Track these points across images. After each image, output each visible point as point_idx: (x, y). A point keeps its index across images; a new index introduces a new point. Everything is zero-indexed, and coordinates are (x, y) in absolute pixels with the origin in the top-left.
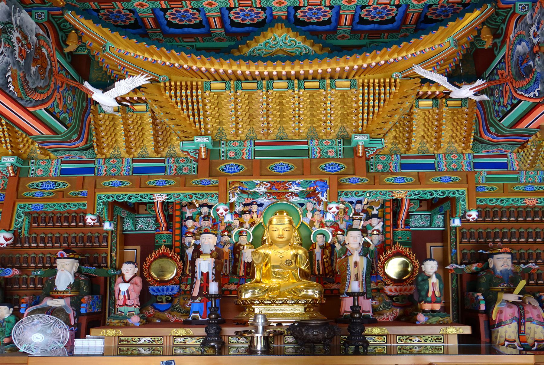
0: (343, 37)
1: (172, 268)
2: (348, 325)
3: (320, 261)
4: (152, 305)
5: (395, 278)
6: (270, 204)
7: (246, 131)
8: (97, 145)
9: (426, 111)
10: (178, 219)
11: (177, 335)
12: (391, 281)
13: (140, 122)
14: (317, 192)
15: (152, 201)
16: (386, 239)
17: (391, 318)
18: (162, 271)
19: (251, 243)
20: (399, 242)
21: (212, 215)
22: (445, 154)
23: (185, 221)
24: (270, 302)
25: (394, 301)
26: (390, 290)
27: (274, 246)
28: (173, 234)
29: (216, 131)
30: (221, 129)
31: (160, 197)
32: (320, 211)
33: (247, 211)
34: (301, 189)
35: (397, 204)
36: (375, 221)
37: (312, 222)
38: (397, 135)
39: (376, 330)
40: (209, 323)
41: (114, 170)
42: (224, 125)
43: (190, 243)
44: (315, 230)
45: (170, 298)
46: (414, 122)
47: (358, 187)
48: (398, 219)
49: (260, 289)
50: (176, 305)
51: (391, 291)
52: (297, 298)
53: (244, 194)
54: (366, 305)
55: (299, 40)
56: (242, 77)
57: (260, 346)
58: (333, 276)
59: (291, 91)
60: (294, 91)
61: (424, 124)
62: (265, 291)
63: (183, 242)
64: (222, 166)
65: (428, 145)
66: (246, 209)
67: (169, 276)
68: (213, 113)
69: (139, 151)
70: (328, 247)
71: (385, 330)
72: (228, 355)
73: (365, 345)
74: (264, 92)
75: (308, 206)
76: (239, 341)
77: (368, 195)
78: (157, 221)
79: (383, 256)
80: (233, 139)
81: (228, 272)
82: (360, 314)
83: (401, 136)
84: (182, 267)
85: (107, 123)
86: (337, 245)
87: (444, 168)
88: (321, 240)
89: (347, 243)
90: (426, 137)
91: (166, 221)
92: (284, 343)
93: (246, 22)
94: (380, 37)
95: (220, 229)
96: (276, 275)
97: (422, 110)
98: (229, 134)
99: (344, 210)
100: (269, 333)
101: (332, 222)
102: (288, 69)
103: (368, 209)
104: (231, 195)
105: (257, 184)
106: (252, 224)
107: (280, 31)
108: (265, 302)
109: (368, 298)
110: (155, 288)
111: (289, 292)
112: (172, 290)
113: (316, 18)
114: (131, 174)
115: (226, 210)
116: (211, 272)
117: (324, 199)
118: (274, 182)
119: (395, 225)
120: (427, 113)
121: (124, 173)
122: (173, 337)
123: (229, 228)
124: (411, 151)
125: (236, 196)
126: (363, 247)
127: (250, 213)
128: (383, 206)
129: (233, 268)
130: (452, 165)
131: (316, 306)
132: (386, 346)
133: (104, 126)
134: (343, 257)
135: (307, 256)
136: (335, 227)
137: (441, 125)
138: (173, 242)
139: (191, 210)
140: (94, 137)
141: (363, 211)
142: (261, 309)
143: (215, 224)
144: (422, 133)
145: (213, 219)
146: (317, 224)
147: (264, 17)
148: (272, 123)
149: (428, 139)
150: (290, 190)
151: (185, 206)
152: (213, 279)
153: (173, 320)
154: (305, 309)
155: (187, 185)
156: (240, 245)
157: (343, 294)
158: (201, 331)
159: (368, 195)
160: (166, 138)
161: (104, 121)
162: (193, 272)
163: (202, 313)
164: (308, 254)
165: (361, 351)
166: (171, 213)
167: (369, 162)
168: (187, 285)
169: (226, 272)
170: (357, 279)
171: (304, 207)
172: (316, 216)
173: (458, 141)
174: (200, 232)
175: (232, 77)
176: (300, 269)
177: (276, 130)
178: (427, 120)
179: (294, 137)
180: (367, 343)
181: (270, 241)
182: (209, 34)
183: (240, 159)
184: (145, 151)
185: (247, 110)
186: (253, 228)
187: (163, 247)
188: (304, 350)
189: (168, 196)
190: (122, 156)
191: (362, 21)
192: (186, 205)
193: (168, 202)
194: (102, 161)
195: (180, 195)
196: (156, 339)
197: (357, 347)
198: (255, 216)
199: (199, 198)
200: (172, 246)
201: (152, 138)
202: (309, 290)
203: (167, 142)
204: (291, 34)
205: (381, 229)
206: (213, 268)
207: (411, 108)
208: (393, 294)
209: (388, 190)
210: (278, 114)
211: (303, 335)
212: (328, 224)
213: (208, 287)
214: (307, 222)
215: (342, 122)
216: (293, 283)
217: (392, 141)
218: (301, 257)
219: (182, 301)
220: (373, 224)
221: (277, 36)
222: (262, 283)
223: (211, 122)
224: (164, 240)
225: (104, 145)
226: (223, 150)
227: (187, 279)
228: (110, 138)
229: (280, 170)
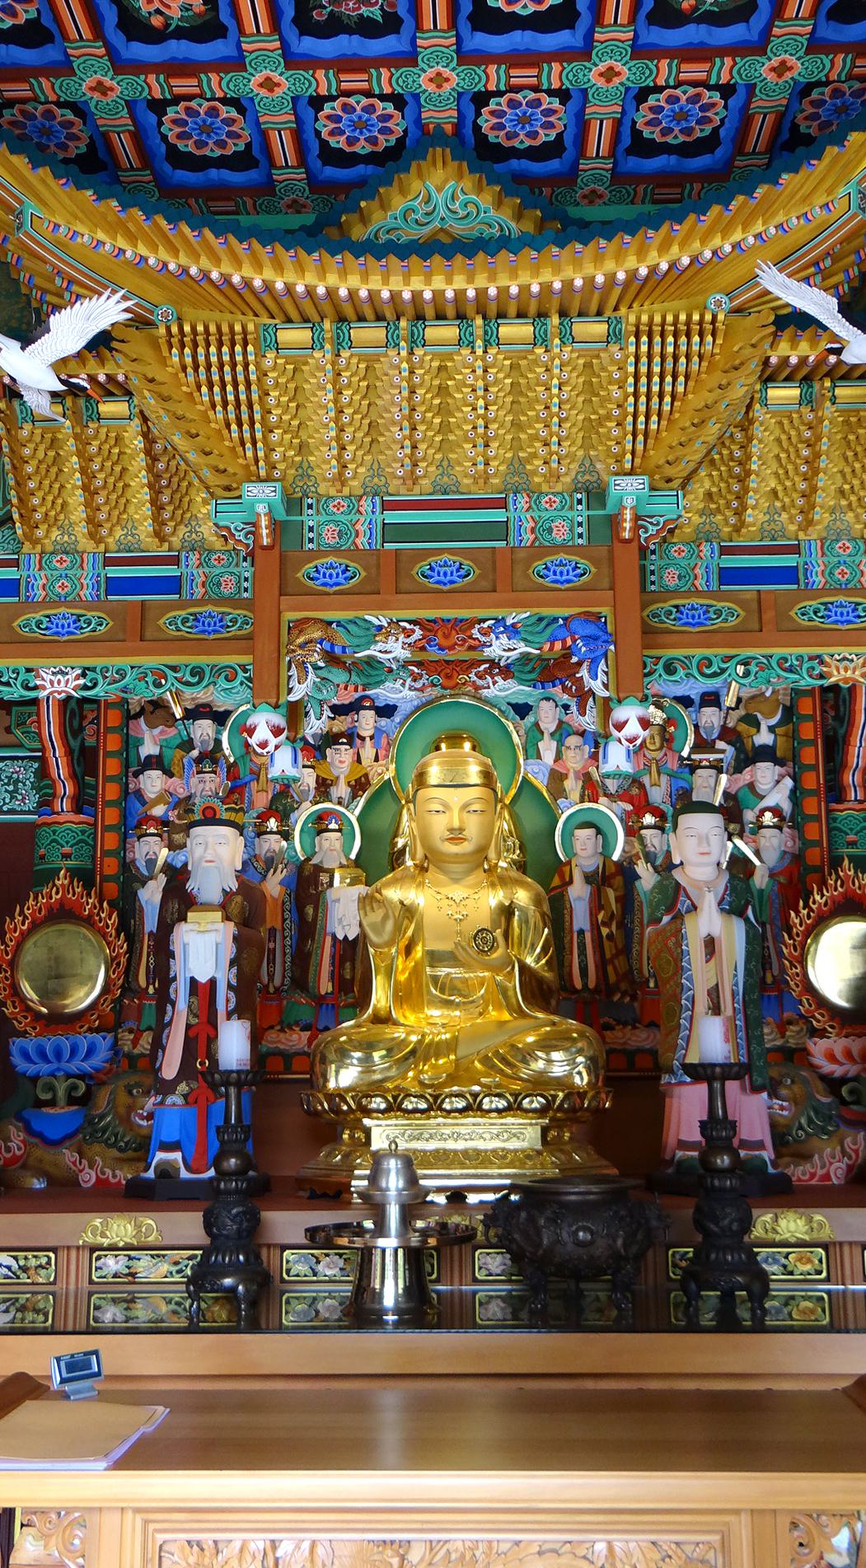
0: (592, 197)
1: (91, 960)
2: (693, 1201)
3: (588, 936)
4: (19, 1118)
5: (843, 1004)
6: (418, 708)
7: (362, 470)
8: (21, 515)
9: (784, 415)
10: (112, 767)
11: (106, 1242)
12: (832, 1019)
13: (116, 450)
14: (575, 659)
15: (32, 694)
16: (806, 844)
17: (837, 1171)
18: (56, 979)
19: (357, 863)
20: (852, 858)
21: (227, 752)
22: (823, 540)
23: (136, 775)
24: (423, 1105)
25: (843, 1102)
26: (829, 1052)
27: (433, 873)
28: (95, 825)
29: (293, 471)
30: (305, 465)
31: (57, 681)
32: (582, 734)
33: (342, 735)
34: (523, 648)
35: (836, 707)
36: (765, 773)
37: (557, 778)
38: (714, 490)
39: (792, 1225)
40: (218, 1192)
41: (63, 586)
42: (312, 454)
43: (151, 863)
44: (568, 810)
45: (82, 1087)
47: (708, 639)
48: (844, 765)
49: (389, 1050)
50: (102, 1117)
51: (831, 1057)
52: (516, 1087)
53: (334, 670)
54: (753, 1114)
55: (485, 200)
56: (349, 311)
57: (391, 1290)
58: (634, 997)
59: (466, 352)
60: (473, 352)
61: (777, 457)
62: (406, 1058)
63: (130, 856)
64: (309, 568)
65: (784, 516)
66: (341, 724)
67: (82, 997)
68: (286, 417)
69: (119, 533)
70: (613, 876)
71: (821, 1225)
72: (281, 1329)
73: (756, 1287)
74: (404, 353)
75: (542, 714)
76: (320, 1268)
77: (741, 669)
78: (43, 773)
79: (797, 913)
80: (333, 492)
81: (277, 981)
82: (734, 1153)
83: (724, 492)
84: (123, 960)
85: (40, 454)
86: (642, 868)
87: (818, 580)
88: (590, 851)
89: (676, 861)
90: (781, 494)
91: (73, 775)
92: (475, 1281)
93: (357, 149)
94: (682, 194)
95: (251, 804)
96: (442, 991)
97: (774, 414)
98: (324, 479)
99: (663, 729)
100: (425, 1233)
101: (627, 776)
103: (742, 727)
104: (294, 671)
105: (380, 628)
106: (359, 785)
107: (439, 174)
108: (408, 1105)
109: (756, 1090)
110: (30, 1044)
111: (485, 1060)
112: (90, 1052)
113: (528, 135)
114: (102, 597)
115: (277, 732)
116: (225, 977)
117: (597, 686)
118: (434, 621)
119: (835, 792)
120: (786, 422)
121: (86, 594)
122: (93, 1249)
123: (283, 801)
124: (744, 530)
125: (311, 676)
126: (732, 877)
127: (350, 743)
128: (789, 713)
129: (301, 969)
130: (837, 571)
131: (576, 1121)
132: (829, 1292)
133: (34, 463)
134: (666, 919)
135: (543, 915)
136: (634, 795)
137: (817, 455)
138: (94, 857)
139: (156, 731)
140: (13, 492)
141: (726, 733)
142: (393, 1132)
143: (236, 790)
144: (773, 484)
145: (230, 766)
146: (572, 786)
147: (399, 131)
148: (422, 447)
149: (787, 500)
150: (488, 652)
151: (137, 716)
152: (232, 1006)
153: (88, 1178)
154: (545, 1131)
155: (148, 635)
156: (319, 869)
157: (671, 1071)
158: (188, 1226)
159: (741, 669)
160: (178, 496)
161: (32, 446)
162: (163, 975)
163: (191, 1149)
164: (546, 908)
165: (743, 1313)
166: (90, 742)
167: (647, 563)
168: (138, 1034)
169: (271, 977)
170: (716, 1010)
171: (530, 719)
172: (570, 754)
173: (854, 505)
174: (188, 817)
175: (327, 307)
176: (524, 968)
177: (432, 469)
178: (785, 444)
179: (473, 488)
180: (763, 1277)
181: (420, 853)
182: (268, 187)
183: (349, 550)
184: (133, 535)
185: (364, 409)
186: (362, 802)
187: (62, 880)
188: (545, 1307)
189: (84, 675)
190: (80, 548)
191: (642, 147)
192: (142, 712)
193: (85, 700)
194: (35, 560)
195: (128, 674)
196: (33, 1262)
197: (728, 1297)
198: (368, 752)
199: (188, 684)
200: (93, 872)
201: (145, 495)
202: (556, 1055)
203: (181, 504)
204: (468, 182)
205: (786, 807)
206: (232, 963)
207: (749, 407)
208: (838, 1071)
209: (805, 651)
210: (437, 421)
211: (540, 1244)
212: (612, 785)
213: (213, 1038)
214: (537, 774)
215: (586, 445)
216: (502, 1024)
217: (701, 506)
218: (525, 921)
219: (123, 1099)
220: (762, 787)
221: (432, 189)
222: (396, 1023)
223: (281, 444)
224: (67, 849)
225: (38, 516)
226: (311, 523)
227: (140, 1008)
228: (50, 498)
229: (442, 578)
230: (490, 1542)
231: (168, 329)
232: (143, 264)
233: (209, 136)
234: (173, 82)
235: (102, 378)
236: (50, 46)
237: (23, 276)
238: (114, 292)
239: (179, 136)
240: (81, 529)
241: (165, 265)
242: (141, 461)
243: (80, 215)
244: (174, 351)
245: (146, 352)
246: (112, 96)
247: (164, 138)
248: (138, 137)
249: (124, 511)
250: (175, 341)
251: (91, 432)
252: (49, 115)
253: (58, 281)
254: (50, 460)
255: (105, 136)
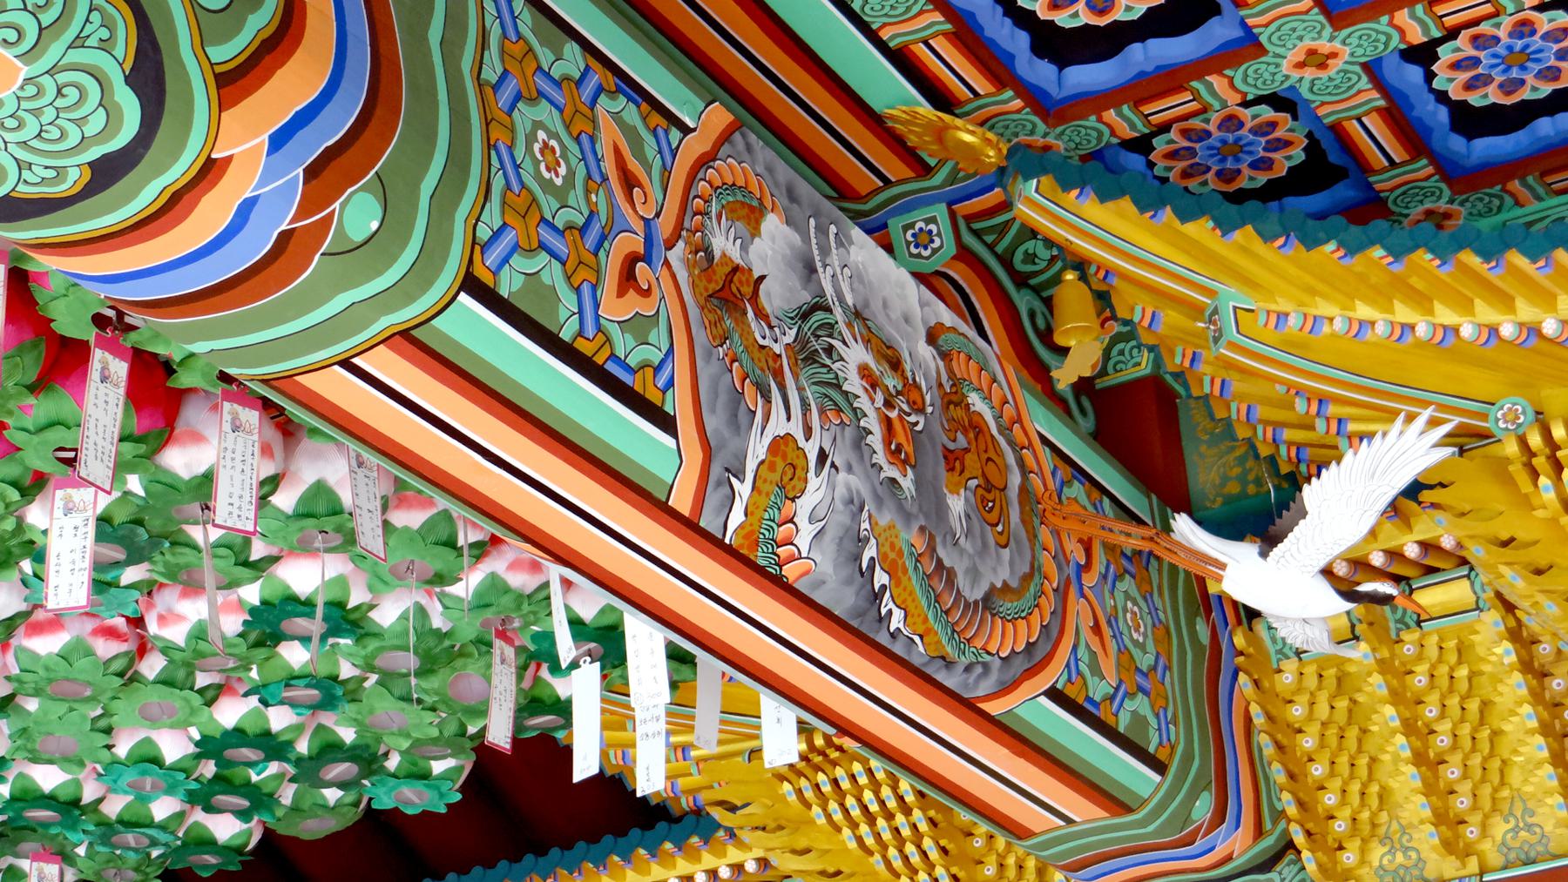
8: (1309, 834)
13: (1463, 672)
85: (1322, 710)
133: (1314, 729)
140: (1286, 796)
161: (1305, 698)
184: (1529, 827)
225: (1340, 826)
228: (1355, 787)
231: (1523, 441)
232: (1451, 339)
233: (1523, 68)
234: (1441, 10)
235: (1412, 551)
236: (1215, 20)
237: (1236, 410)
238: (1410, 418)
239: (1469, 86)
240: (1426, 839)
241: (1494, 331)
242: (1515, 685)
243: (1320, 286)
244: (1544, 481)
245: (1489, 493)
246: (1336, 65)
247: (1442, 97)
248: (1396, 114)
249: (1503, 783)
250: (1540, 462)
251: (1408, 649)
252: (1232, 122)
253: (1300, 405)
254: (1341, 716)
255: (1337, 130)
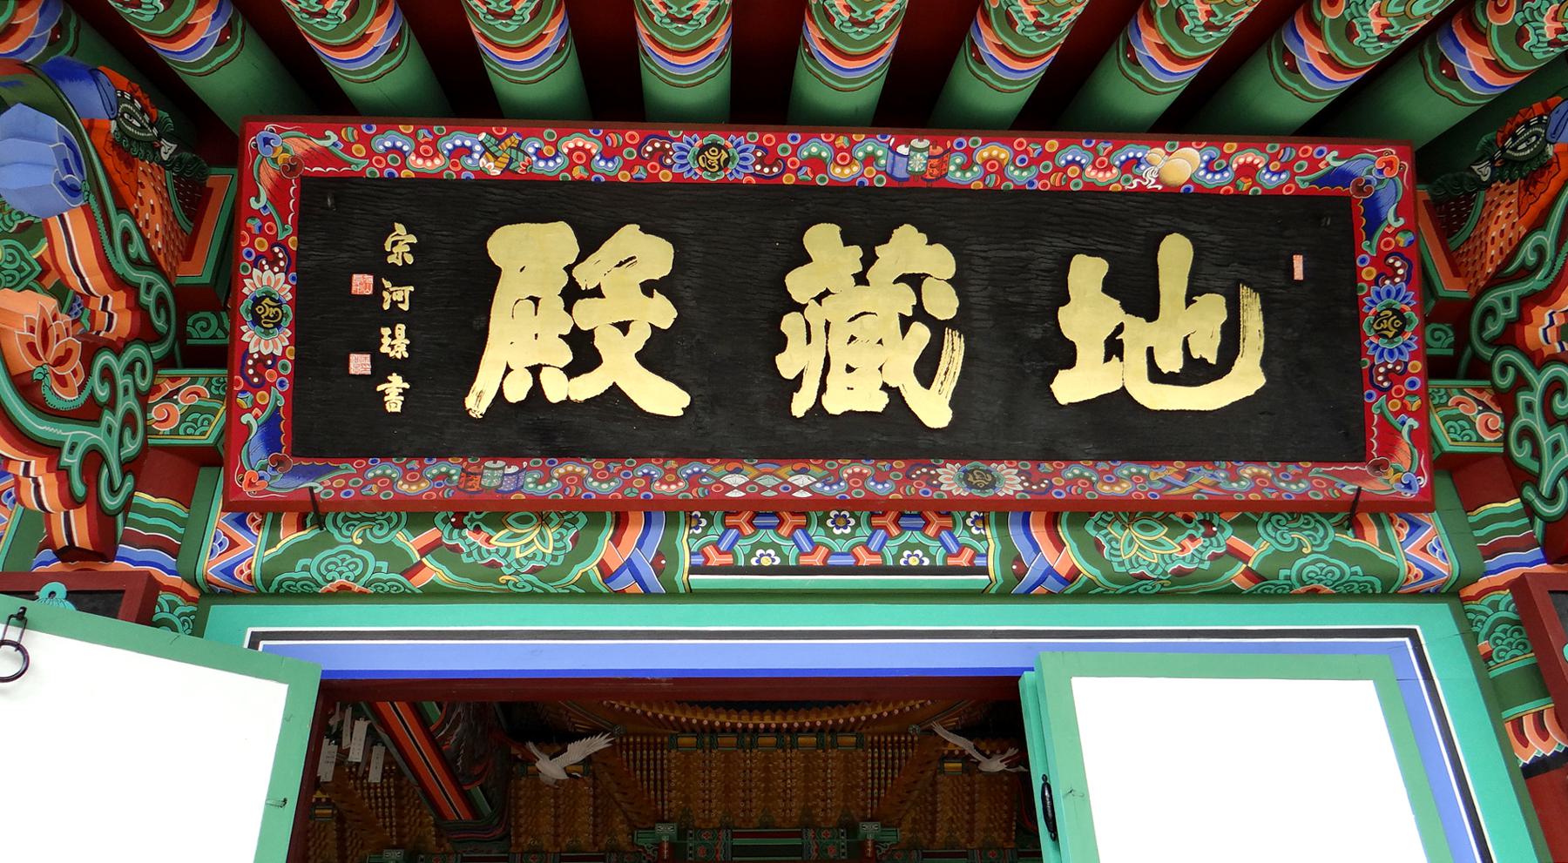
46: (939, 797)
102: (767, 719)
230: (986, 555)
